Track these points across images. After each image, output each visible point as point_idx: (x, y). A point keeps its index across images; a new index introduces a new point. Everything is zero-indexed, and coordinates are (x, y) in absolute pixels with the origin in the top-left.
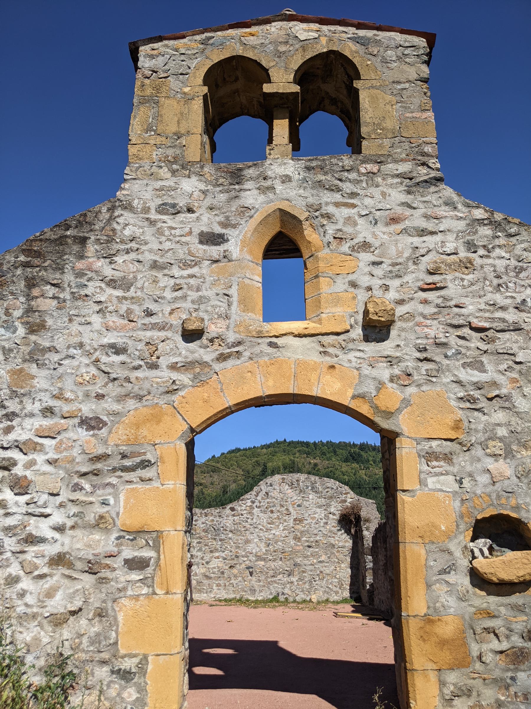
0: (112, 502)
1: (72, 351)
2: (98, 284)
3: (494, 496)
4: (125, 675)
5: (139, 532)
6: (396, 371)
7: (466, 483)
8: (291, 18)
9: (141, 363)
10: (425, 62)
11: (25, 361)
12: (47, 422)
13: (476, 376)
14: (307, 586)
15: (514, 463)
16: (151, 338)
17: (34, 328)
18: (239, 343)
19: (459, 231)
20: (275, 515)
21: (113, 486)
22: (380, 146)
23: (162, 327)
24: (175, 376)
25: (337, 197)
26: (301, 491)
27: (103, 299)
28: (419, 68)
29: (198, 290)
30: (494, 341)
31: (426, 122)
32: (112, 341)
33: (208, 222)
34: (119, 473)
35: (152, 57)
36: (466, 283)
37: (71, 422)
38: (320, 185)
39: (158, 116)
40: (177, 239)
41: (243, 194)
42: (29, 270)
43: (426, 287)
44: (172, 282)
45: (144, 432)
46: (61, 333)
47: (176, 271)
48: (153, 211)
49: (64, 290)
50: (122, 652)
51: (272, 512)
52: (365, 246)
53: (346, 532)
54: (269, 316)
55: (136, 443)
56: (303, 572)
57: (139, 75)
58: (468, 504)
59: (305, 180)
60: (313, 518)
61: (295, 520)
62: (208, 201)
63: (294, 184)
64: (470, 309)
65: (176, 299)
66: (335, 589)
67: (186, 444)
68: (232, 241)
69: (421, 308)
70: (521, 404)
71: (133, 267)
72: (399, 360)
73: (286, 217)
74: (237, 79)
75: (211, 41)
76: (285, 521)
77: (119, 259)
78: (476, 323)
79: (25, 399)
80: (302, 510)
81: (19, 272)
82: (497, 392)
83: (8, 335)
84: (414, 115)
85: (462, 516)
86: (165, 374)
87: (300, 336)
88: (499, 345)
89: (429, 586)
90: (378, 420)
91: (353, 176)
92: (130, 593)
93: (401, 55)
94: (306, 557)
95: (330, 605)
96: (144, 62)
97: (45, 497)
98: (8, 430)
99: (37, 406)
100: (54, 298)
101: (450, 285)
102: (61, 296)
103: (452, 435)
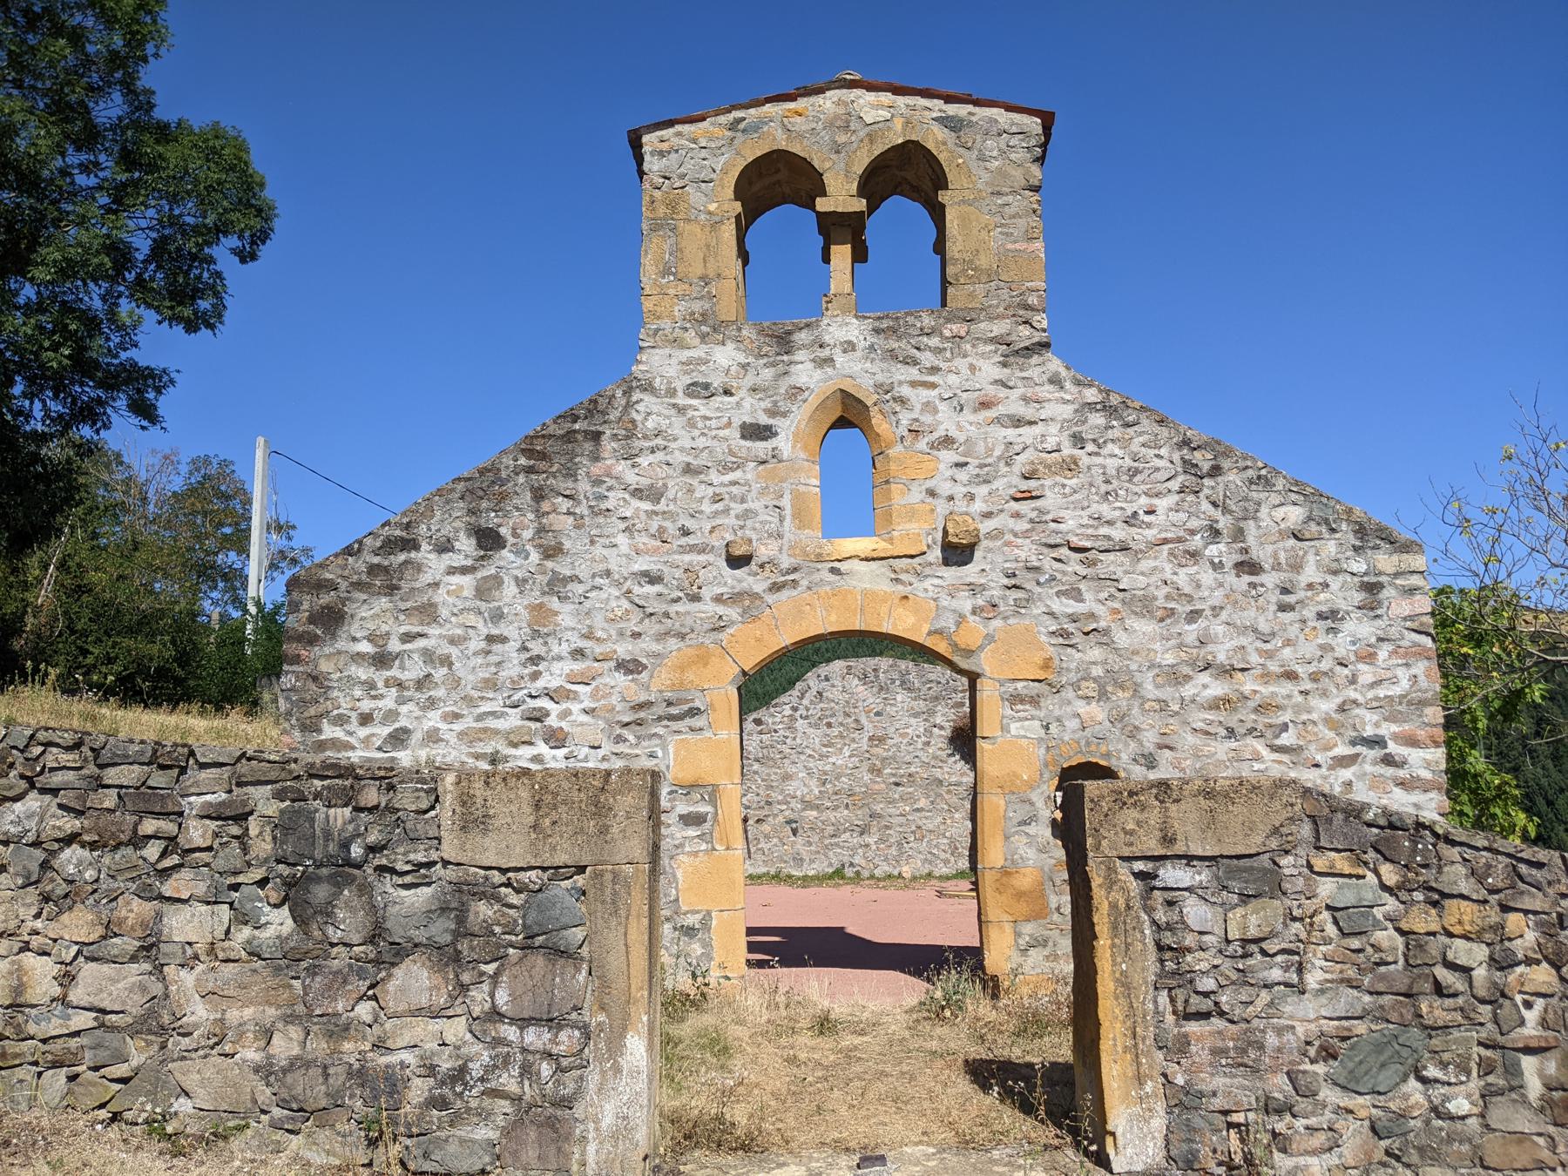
0: (660, 754)
1: (599, 581)
2: (621, 494)
3: (1083, 743)
4: (689, 931)
5: (693, 786)
6: (980, 602)
7: (1053, 729)
8: (853, 85)
9: (681, 594)
10: (1036, 160)
11: (544, 593)
12: (578, 666)
13: (1072, 607)
14: (894, 851)
15: (1108, 705)
16: (690, 564)
17: (552, 552)
18: (795, 570)
19: (1064, 420)
20: (835, 731)
21: (660, 737)
22: (972, 295)
23: (702, 549)
24: (721, 610)
25: (913, 373)
26: (881, 688)
27: (628, 514)
28: (1028, 171)
29: (743, 501)
30: (1095, 564)
31: (1033, 256)
32: (645, 568)
33: (751, 409)
34: (665, 722)
35: (662, 154)
36: (1067, 490)
37: (606, 665)
38: (892, 355)
39: (677, 251)
40: (714, 433)
41: (793, 368)
42: (534, 477)
43: (1020, 495)
44: (710, 491)
45: (690, 676)
46: (580, 560)
47: (714, 476)
48: (680, 393)
49: (579, 503)
50: (684, 908)
51: (829, 725)
52: (947, 441)
53: (963, 758)
54: (833, 529)
55: (680, 686)
56: (887, 827)
57: (646, 185)
58: (1053, 751)
59: (872, 348)
60: (903, 735)
61: (871, 739)
62: (750, 380)
63: (859, 354)
64: (1070, 524)
65: (716, 514)
66: (943, 855)
67: (739, 689)
68: (782, 436)
69: (1011, 523)
70: (1122, 640)
71: (661, 472)
72: (983, 588)
73: (847, 398)
74: (778, 171)
75: (742, 126)
76: (853, 740)
77: (644, 461)
78: (1076, 541)
79: (550, 640)
80: (884, 722)
81: (521, 479)
82: (1094, 626)
83: (519, 561)
84: (1017, 246)
85: (1046, 765)
86: (708, 608)
87: (867, 559)
88: (1101, 570)
89: (1007, 838)
90: (956, 659)
91: (934, 341)
92: (687, 849)
93: (1004, 147)
94: (892, 802)
95: (934, 882)
96: (652, 164)
97: (586, 750)
98: (535, 676)
99: (565, 649)
100: (569, 513)
101: (1048, 493)
102: (578, 511)
103: (1041, 675)
